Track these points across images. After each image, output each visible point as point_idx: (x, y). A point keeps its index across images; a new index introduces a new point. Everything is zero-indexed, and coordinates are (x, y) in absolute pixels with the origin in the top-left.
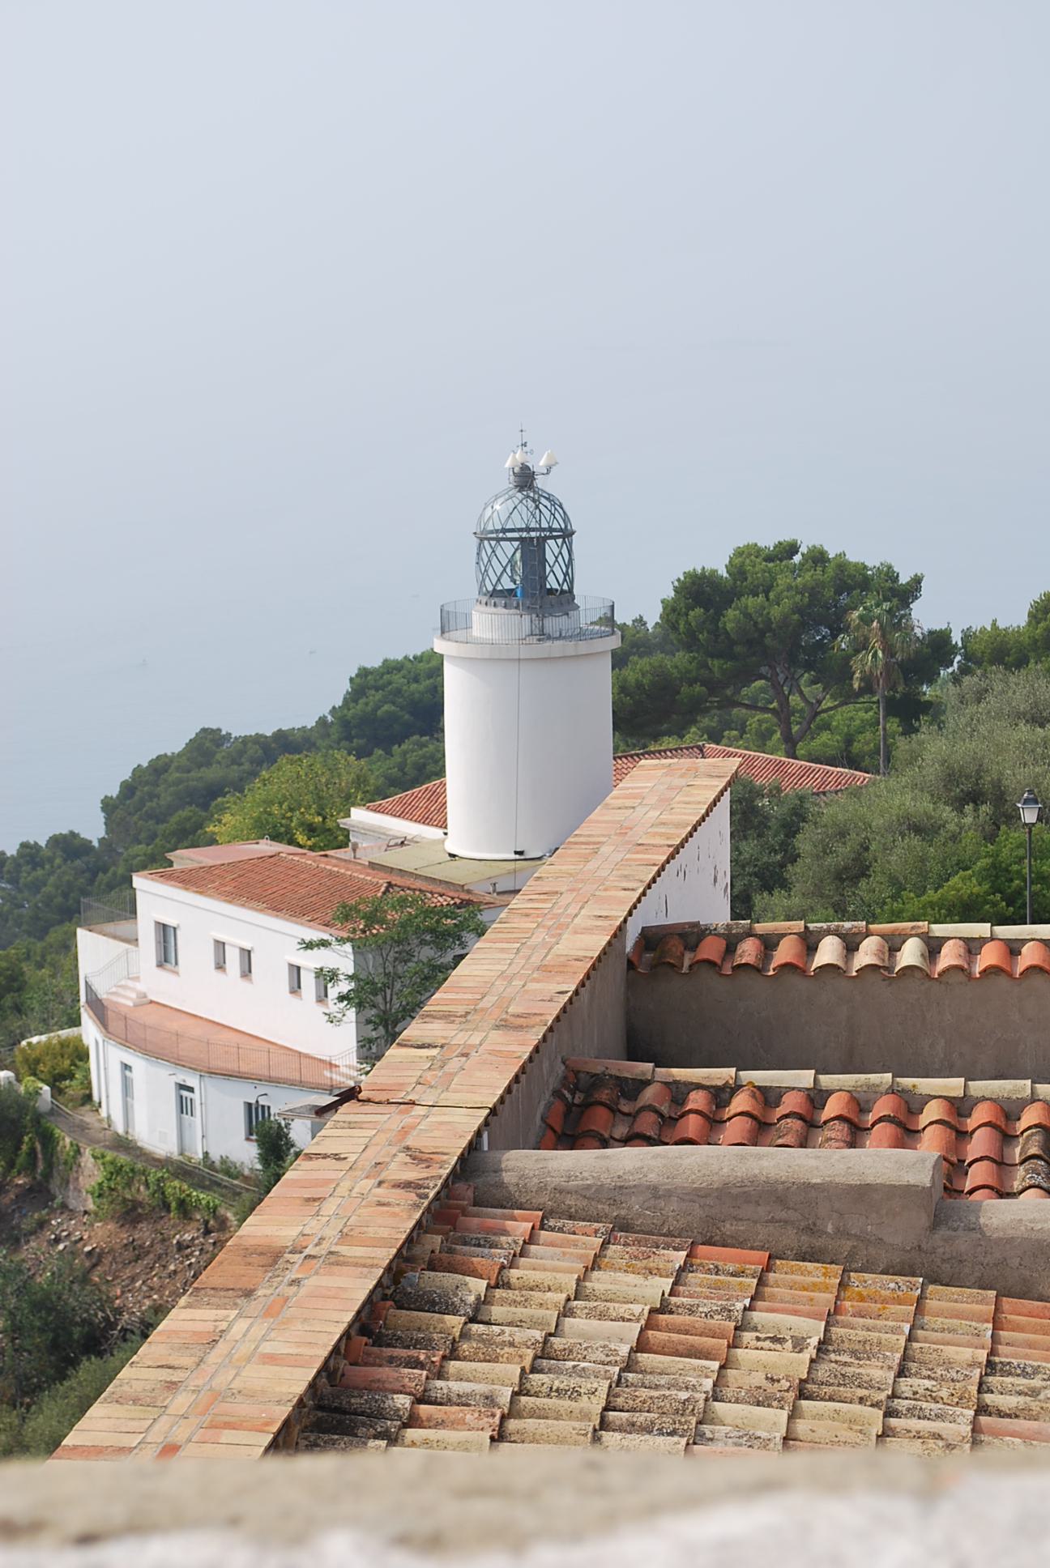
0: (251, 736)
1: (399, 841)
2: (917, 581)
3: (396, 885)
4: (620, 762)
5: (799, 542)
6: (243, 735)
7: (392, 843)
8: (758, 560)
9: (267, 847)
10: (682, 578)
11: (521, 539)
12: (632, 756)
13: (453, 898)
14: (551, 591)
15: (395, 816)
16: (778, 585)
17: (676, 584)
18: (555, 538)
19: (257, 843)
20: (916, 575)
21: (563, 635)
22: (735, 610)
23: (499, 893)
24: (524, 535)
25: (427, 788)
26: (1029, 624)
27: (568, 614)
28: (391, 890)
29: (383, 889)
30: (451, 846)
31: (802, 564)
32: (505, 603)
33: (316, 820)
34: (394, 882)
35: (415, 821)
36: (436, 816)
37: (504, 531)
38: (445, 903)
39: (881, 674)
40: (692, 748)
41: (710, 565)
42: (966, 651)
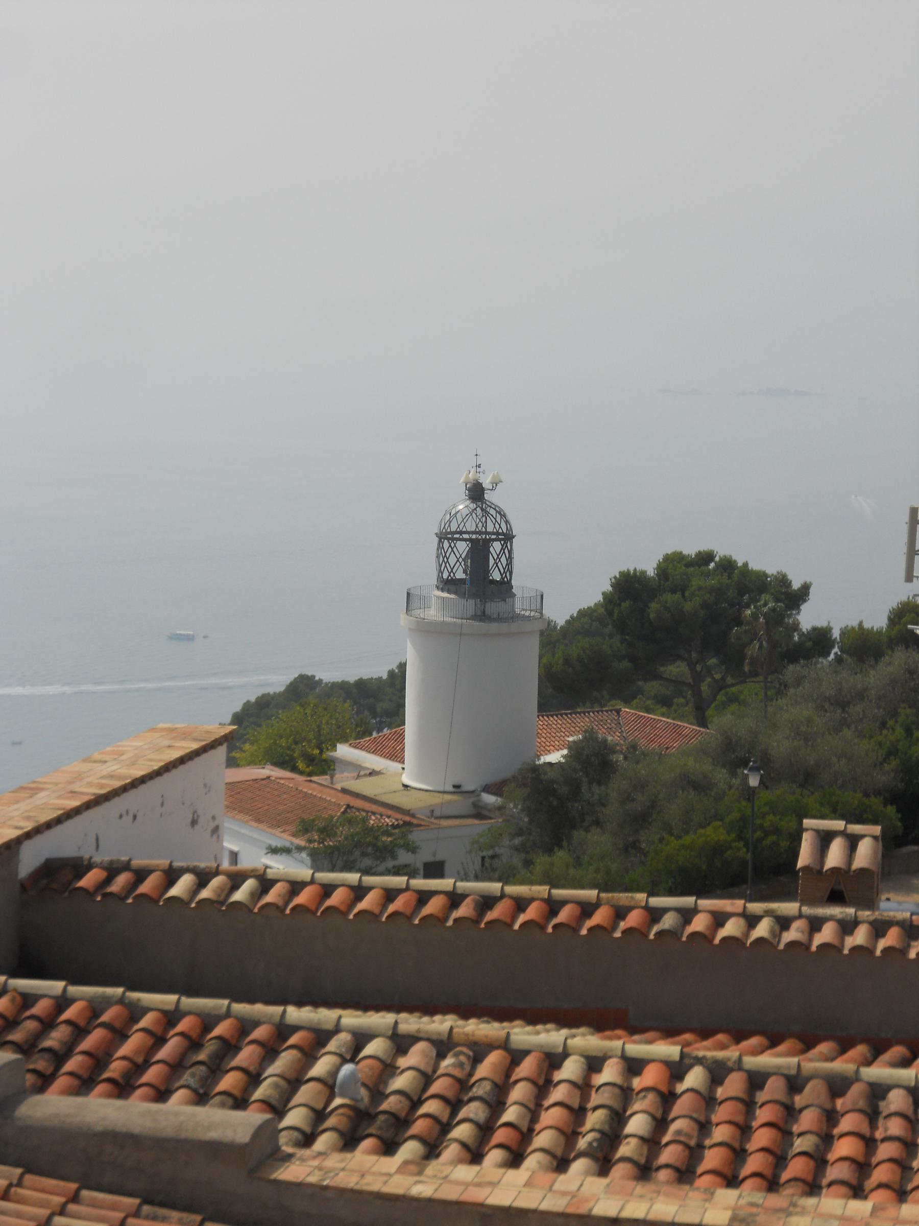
0: (338, 682)
1: (368, 772)
2: (806, 588)
3: (353, 807)
4: (551, 719)
5: (715, 552)
6: (331, 681)
7: (362, 773)
8: (679, 565)
9: (268, 771)
10: (618, 576)
11: (470, 540)
12: (561, 715)
13: (397, 820)
14: (493, 582)
15: (369, 752)
16: (692, 586)
17: (613, 580)
18: (500, 540)
19: (264, 768)
20: (806, 583)
21: (500, 617)
22: (657, 603)
23: (437, 818)
24: (474, 537)
25: (396, 731)
26: (889, 626)
27: (505, 601)
28: (349, 811)
29: (342, 810)
30: (406, 779)
31: (715, 569)
32: (448, 589)
33: (314, 752)
34: (351, 804)
35: (384, 757)
36: (397, 755)
37: (461, 533)
38: (390, 824)
39: (765, 659)
40: (611, 711)
41: (640, 567)
42: (842, 643)
